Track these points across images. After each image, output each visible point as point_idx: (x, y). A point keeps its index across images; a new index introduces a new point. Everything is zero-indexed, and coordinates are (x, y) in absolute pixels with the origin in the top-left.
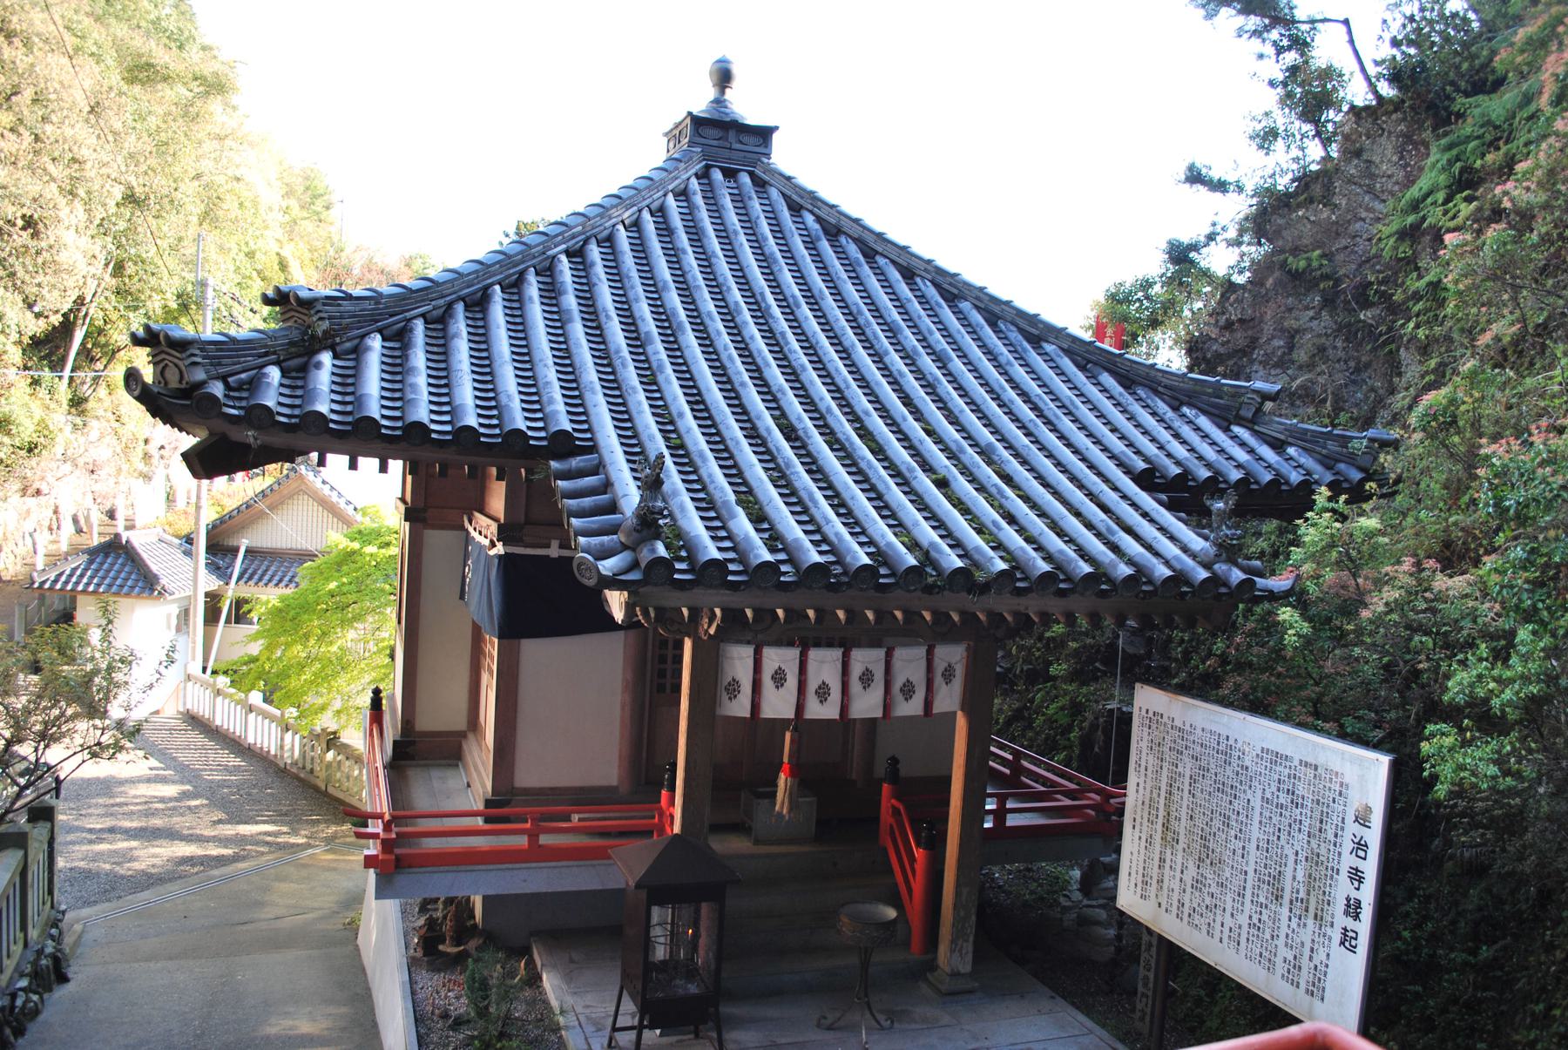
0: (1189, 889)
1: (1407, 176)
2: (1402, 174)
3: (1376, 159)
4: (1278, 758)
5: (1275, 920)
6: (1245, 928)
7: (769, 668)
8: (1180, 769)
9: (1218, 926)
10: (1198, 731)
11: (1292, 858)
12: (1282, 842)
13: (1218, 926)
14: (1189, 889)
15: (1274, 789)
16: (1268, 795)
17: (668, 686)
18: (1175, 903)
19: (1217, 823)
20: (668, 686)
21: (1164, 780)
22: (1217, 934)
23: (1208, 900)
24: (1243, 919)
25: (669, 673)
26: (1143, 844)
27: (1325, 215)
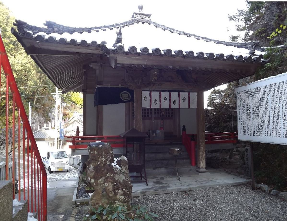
0: (255, 127)
1: (280, 10)
2: (279, 10)
3: (273, 9)
4: (272, 85)
5: (279, 124)
6: (271, 130)
7: (163, 97)
8: (249, 101)
9: (264, 133)
10: (252, 90)
11: (281, 106)
12: (278, 104)
13: (264, 133)
14: (255, 127)
15: (273, 92)
16: (272, 95)
17: (144, 110)
18: (252, 132)
19: (260, 108)
20: (144, 110)
21: (246, 105)
22: (264, 135)
23: (261, 128)
24: (271, 128)
25: (144, 113)
26: (242, 122)
27: (264, 22)
